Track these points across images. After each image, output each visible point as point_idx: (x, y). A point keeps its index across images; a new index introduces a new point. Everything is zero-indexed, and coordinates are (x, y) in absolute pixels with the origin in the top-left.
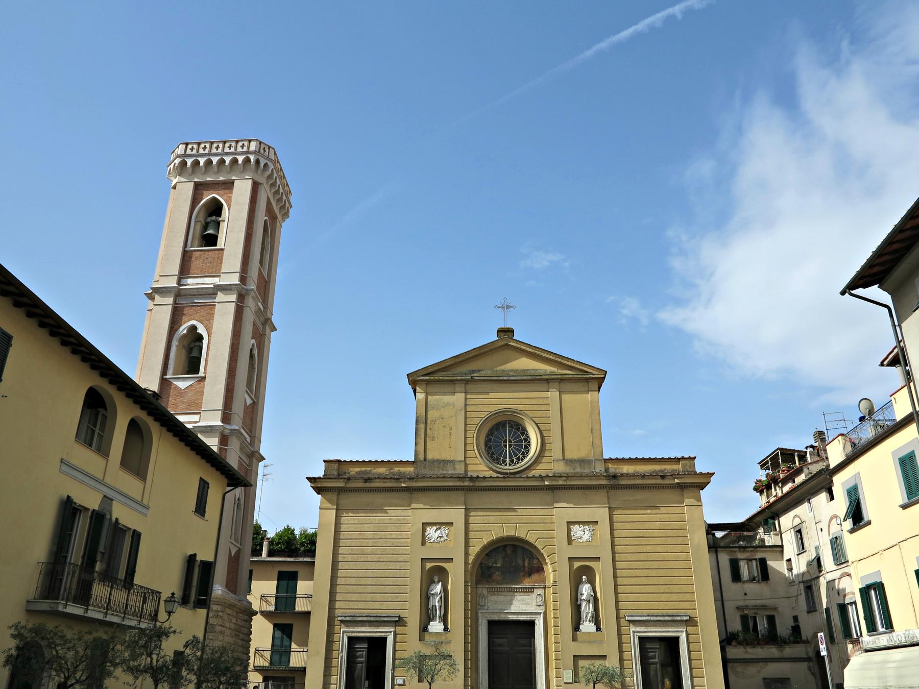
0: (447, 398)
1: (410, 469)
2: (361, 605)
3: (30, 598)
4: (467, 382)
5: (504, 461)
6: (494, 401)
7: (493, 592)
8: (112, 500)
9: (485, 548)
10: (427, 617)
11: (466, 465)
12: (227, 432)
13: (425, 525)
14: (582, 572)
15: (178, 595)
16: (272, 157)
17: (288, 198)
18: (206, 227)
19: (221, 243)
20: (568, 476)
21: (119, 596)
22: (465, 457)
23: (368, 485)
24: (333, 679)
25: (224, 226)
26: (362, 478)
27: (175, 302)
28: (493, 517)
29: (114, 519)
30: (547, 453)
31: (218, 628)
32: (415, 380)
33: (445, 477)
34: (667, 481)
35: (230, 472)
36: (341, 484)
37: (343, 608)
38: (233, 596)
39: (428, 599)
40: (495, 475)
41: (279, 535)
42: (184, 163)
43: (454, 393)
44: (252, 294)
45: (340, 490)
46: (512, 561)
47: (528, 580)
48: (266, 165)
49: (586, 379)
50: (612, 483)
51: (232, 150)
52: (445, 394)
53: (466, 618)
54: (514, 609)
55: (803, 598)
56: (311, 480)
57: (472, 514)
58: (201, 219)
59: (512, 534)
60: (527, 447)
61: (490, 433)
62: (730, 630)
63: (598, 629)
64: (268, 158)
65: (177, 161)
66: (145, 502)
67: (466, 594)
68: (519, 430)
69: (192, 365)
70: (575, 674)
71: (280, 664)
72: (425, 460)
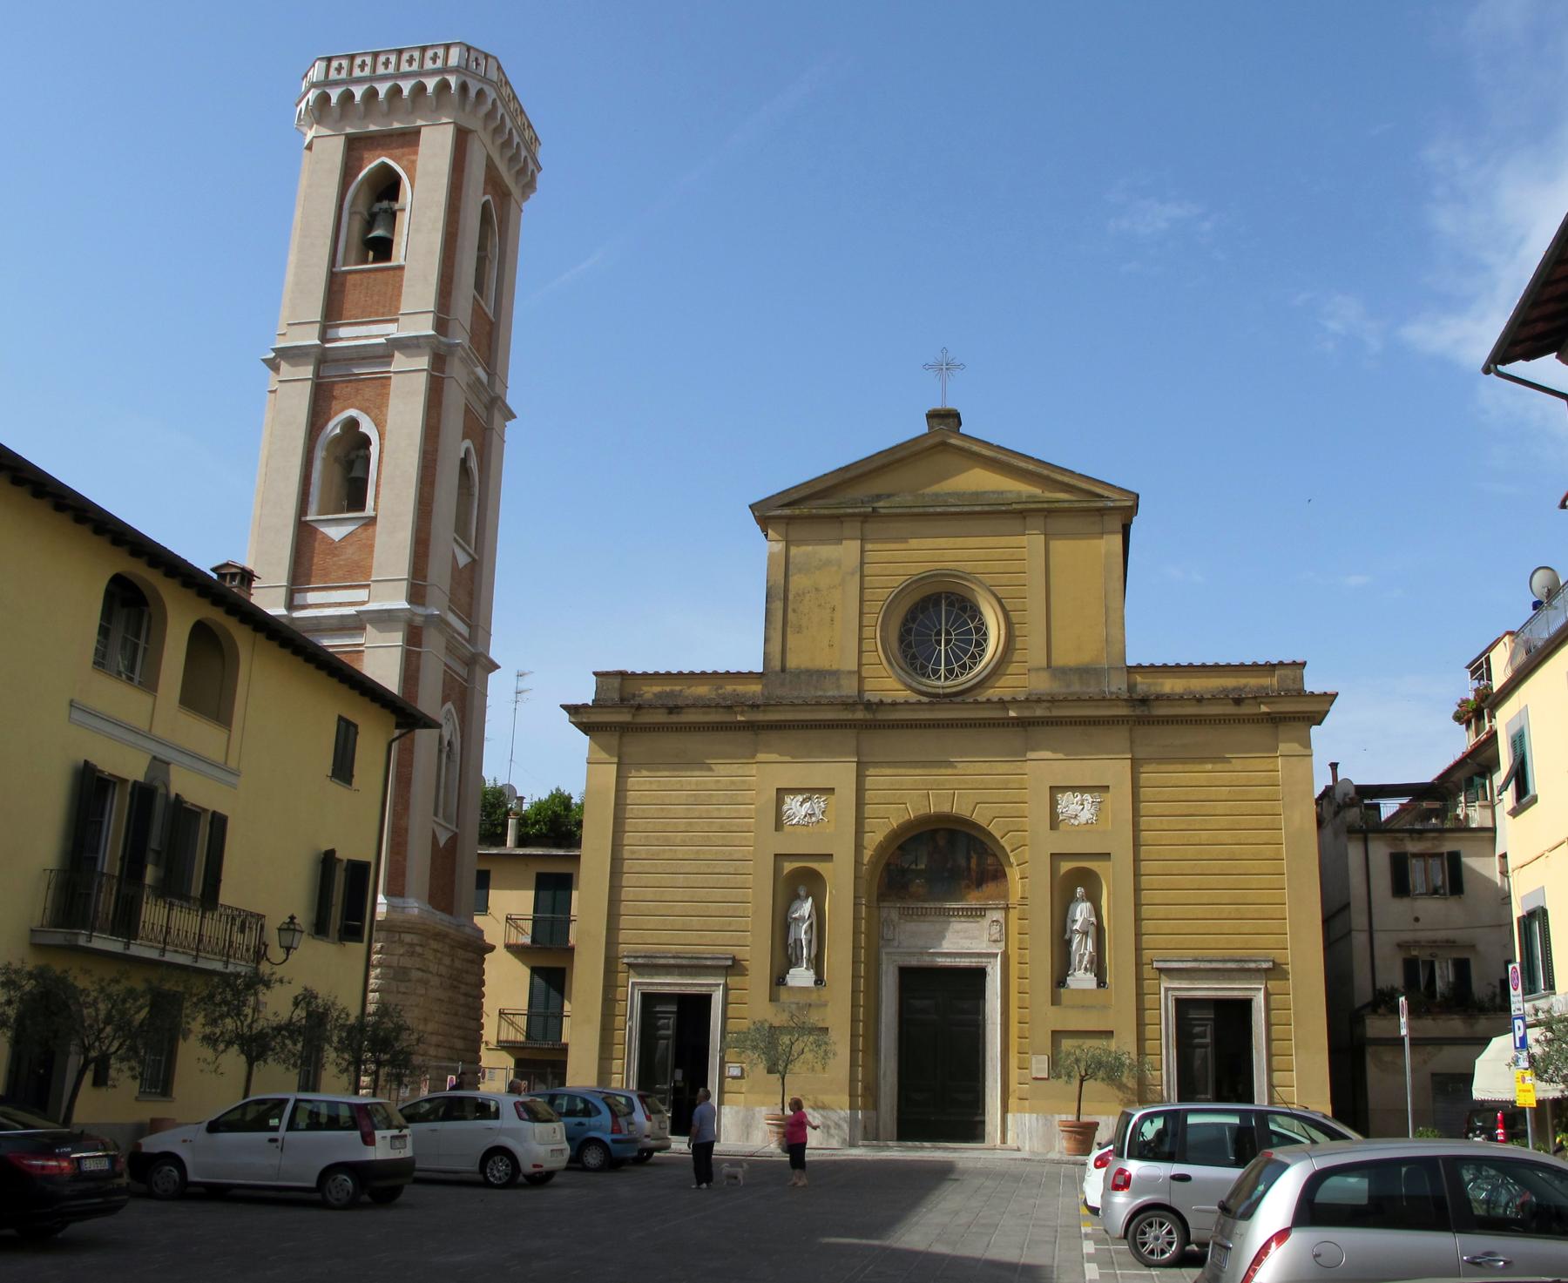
0: (827, 551)
1: (755, 688)
2: (665, 936)
3: (35, 924)
4: (865, 518)
5: (936, 672)
6: (916, 555)
8: (168, 764)
9: (894, 835)
10: (785, 958)
11: (861, 679)
12: (418, 621)
13: (781, 793)
14: (1075, 880)
15: (304, 919)
16: (493, 75)
17: (536, 162)
18: (370, 224)
19: (399, 255)
20: (1053, 701)
21: (185, 920)
22: (860, 665)
23: (674, 718)
24: (617, 1065)
25: (403, 220)
26: (663, 706)
27: (317, 374)
28: (912, 777)
29: (173, 795)
30: (1017, 656)
31: (416, 975)
32: (770, 514)
33: (818, 704)
34: (1246, 709)
36: (624, 717)
37: (632, 942)
38: (445, 917)
39: (787, 927)
40: (914, 698)
41: (539, 807)
42: (324, 99)
43: (839, 541)
44: (460, 352)
45: (623, 729)
46: (941, 859)
47: (976, 893)
48: (480, 93)
49: (1099, 510)
50: (1138, 712)
51: (415, 66)
52: (822, 542)
53: (855, 962)
54: (947, 946)
56: (572, 710)
57: (871, 771)
58: (362, 207)
59: (946, 809)
61: (912, 615)
62: (1380, 984)
63: (1101, 983)
64: (485, 79)
65: (312, 95)
66: (232, 764)
67: (856, 918)
68: (965, 608)
69: (353, 493)
70: (1054, 1063)
71: (545, 1038)
72: (783, 670)
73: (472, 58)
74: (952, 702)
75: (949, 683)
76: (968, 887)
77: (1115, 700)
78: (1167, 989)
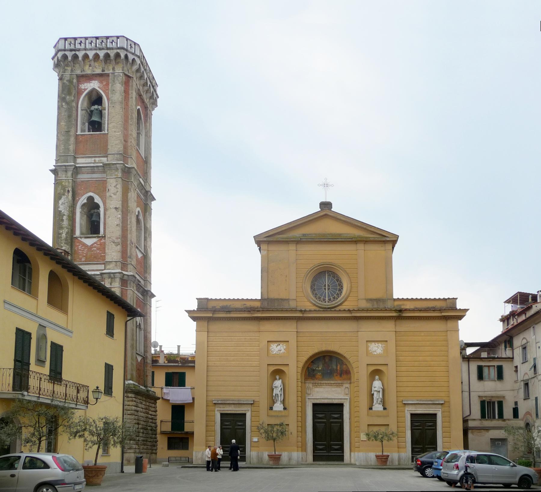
1: (258, 304)
5: (324, 300)
7: (316, 385)
15: (102, 388)
16: (138, 53)
17: (157, 94)
18: (91, 113)
20: (367, 310)
35: (127, 307)
40: (317, 309)
55: (522, 391)
60: (341, 290)
66: (69, 328)
73: (129, 44)
74: (331, 311)
75: (329, 304)
76: (337, 375)
77: (391, 310)
78: (408, 410)
